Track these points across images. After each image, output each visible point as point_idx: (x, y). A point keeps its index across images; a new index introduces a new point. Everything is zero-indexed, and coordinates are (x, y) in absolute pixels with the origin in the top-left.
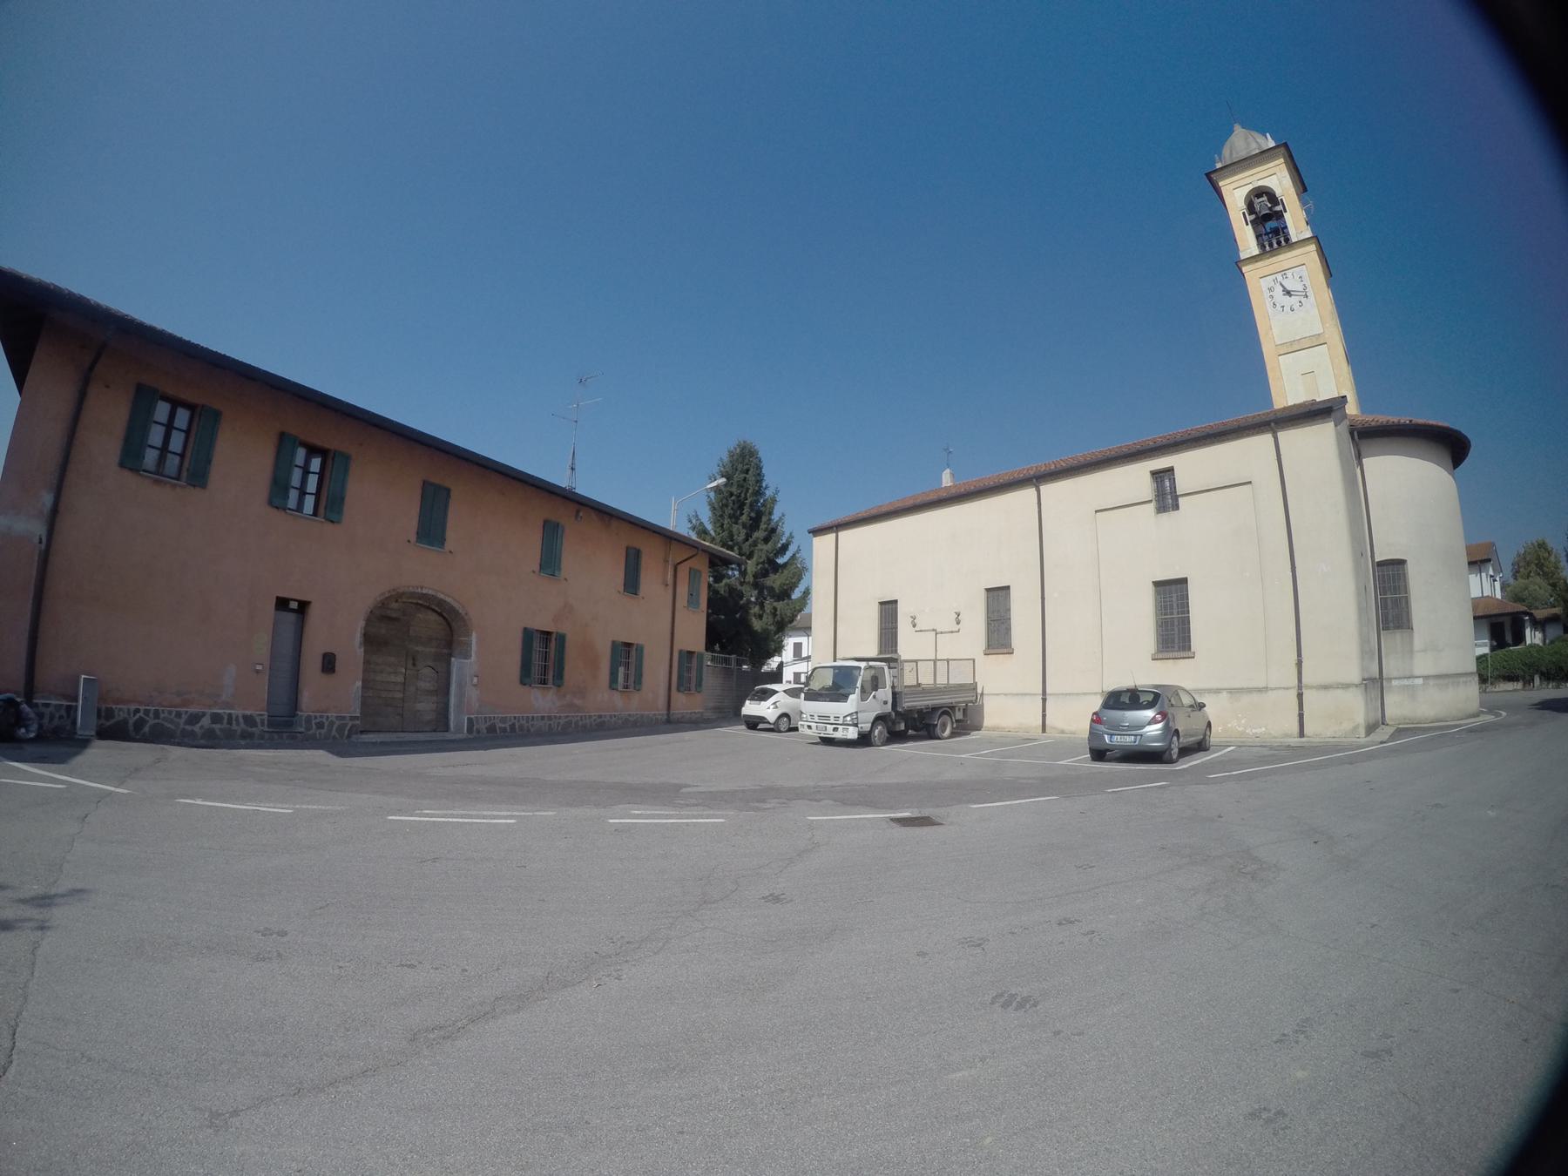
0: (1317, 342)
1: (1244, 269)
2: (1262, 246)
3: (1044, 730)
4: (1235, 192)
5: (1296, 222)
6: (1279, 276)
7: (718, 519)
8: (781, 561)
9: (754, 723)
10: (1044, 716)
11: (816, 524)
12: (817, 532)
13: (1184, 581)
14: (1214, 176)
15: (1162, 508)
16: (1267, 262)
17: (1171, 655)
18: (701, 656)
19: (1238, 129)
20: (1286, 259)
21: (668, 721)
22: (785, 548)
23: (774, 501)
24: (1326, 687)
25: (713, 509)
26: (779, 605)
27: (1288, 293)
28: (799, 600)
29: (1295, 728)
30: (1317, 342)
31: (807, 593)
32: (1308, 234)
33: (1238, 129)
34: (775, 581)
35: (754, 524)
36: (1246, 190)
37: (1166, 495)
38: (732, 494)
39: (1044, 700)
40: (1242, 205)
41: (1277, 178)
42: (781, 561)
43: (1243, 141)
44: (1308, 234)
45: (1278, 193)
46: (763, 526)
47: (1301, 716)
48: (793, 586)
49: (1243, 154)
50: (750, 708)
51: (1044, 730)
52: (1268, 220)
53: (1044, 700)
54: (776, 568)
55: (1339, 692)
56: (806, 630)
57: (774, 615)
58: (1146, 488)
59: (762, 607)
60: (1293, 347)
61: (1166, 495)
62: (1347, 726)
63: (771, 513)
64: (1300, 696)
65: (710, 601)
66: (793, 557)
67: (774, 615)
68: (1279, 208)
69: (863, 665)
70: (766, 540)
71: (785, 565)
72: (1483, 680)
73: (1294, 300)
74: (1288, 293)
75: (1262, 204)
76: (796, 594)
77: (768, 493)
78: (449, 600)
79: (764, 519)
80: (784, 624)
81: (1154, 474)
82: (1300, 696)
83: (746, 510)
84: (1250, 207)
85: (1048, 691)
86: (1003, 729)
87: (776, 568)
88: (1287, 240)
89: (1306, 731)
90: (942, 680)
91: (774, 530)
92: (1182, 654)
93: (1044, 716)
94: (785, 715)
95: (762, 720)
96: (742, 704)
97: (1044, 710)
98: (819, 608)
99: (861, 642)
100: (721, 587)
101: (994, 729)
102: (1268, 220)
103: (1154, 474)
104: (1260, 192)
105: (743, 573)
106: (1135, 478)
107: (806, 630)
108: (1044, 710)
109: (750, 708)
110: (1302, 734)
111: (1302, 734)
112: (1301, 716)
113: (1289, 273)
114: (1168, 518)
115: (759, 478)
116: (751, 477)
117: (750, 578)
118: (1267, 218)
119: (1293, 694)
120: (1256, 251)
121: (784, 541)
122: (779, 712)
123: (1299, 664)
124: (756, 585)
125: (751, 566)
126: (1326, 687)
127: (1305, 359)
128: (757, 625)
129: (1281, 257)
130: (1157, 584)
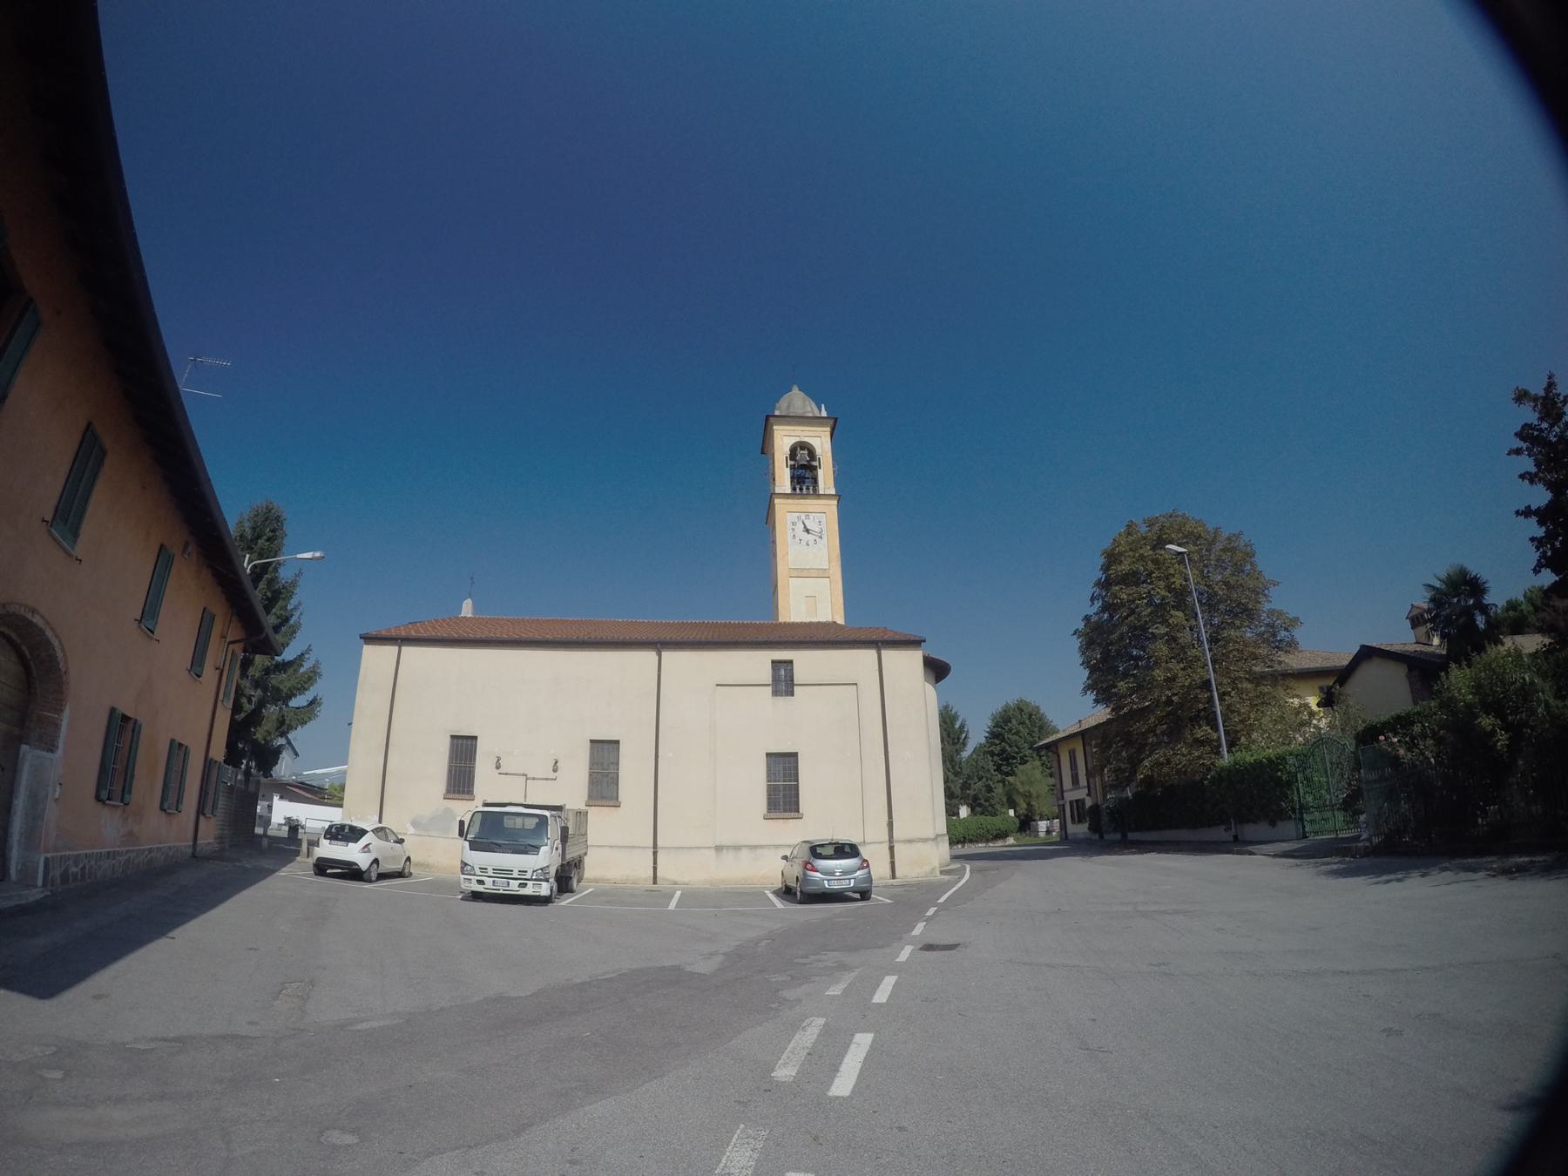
0: (822, 574)
1: (777, 501)
4: (784, 439)
5: (826, 478)
10: (655, 869)
11: (373, 631)
12: (370, 639)
13: (795, 755)
15: (776, 693)
19: (795, 390)
20: (811, 504)
21: (194, 856)
24: (910, 841)
27: (807, 531)
29: (888, 872)
30: (822, 574)
32: (833, 492)
33: (795, 390)
36: (794, 440)
37: (783, 681)
39: (655, 854)
40: (787, 450)
41: (821, 441)
43: (797, 400)
44: (833, 492)
45: (818, 451)
47: (893, 864)
49: (800, 412)
52: (804, 474)
53: (655, 854)
55: (920, 845)
58: (766, 675)
60: (802, 573)
61: (783, 681)
62: (927, 868)
64: (891, 848)
69: (547, 813)
72: (952, 843)
74: (807, 531)
76: (298, 701)
78: (56, 643)
79: (280, 603)
81: (776, 664)
82: (891, 848)
83: (262, 585)
88: (815, 490)
89: (898, 874)
91: (287, 620)
93: (655, 869)
101: (596, 881)
102: (804, 474)
103: (776, 664)
106: (758, 663)
110: (894, 876)
111: (894, 876)
112: (893, 864)
114: (782, 701)
118: (802, 467)
119: (886, 846)
120: (789, 491)
122: (371, 857)
123: (890, 825)
126: (910, 841)
127: (810, 585)
130: (768, 755)
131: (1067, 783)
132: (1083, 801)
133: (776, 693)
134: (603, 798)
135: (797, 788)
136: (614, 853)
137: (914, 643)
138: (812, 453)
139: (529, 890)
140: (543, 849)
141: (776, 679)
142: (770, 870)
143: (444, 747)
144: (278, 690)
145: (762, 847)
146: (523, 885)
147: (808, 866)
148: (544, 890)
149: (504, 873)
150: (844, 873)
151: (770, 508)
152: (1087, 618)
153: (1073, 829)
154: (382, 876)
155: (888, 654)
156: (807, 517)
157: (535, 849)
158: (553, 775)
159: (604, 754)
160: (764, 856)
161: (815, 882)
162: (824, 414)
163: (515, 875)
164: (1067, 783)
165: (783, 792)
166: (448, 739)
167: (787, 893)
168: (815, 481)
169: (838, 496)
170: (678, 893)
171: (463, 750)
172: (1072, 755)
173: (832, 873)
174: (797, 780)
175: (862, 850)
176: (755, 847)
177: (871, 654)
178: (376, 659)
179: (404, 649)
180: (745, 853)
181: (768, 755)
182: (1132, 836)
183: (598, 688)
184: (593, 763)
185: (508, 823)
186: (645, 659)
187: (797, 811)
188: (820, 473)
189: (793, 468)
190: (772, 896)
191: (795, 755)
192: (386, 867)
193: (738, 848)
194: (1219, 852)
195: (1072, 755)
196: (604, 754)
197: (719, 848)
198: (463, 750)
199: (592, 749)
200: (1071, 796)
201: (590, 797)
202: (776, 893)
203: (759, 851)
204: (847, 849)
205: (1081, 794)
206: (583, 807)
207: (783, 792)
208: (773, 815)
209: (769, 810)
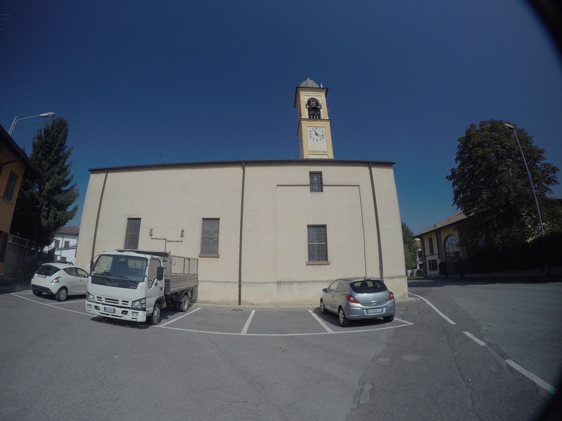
2: (310, 117)
3: (240, 304)
4: (304, 97)
5: (324, 113)
6: (314, 128)
7: (36, 153)
8: (63, 189)
9: (41, 292)
10: (240, 295)
12: (94, 171)
13: (324, 226)
14: (299, 89)
16: (308, 122)
17: (320, 262)
18: (6, 236)
19: (308, 79)
20: (318, 123)
22: (67, 182)
23: (69, 153)
24: (392, 278)
25: (35, 146)
26: (59, 213)
27: (317, 135)
28: (71, 212)
31: (76, 209)
34: (59, 198)
35: (54, 163)
38: (47, 142)
39: (240, 286)
40: (306, 101)
41: (321, 98)
42: (63, 189)
43: (310, 83)
45: (320, 102)
46: (60, 165)
48: (69, 204)
50: (38, 280)
51: (240, 304)
52: (314, 110)
53: (240, 286)
54: (61, 192)
56: (75, 234)
57: (55, 218)
58: (307, 181)
59: (48, 212)
63: (66, 159)
65: (18, 201)
66: (72, 188)
67: (55, 218)
68: (319, 107)
69: (148, 257)
70: (59, 174)
71: (66, 191)
73: (318, 138)
74: (317, 135)
75: (313, 104)
76: (70, 209)
77: (66, 150)
79: (61, 161)
80: (57, 226)
81: (312, 174)
83: (53, 153)
84: (309, 102)
85: (242, 280)
86: (211, 302)
87: (61, 192)
88: (319, 118)
90: (186, 272)
91: (65, 169)
92: (324, 262)
93: (240, 295)
94: (64, 288)
95: (47, 290)
96: (32, 277)
97: (240, 291)
98: (86, 220)
99: (113, 243)
100: (27, 193)
101: (205, 302)
102: (314, 110)
103: (312, 174)
104: (313, 100)
105: (41, 191)
106: (301, 173)
107: (75, 234)
108: (240, 291)
109: (38, 280)
113: (318, 128)
114: (316, 195)
115: (65, 138)
116: (61, 136)
117: (44, 193)
120: (308, 117)
121: (67, 178)
122: (59, 286)
124: (47, 198)
125: (48, 186)
126: (392, 278)
128: (44, 223)
129: (317, 122)
130: (309, 226)
131: (428, 252)
132: (435, 261)
133: (312, 190)
134: (210, 252)
135: (326, 246)
136: (214, 286)
137: (388, 164)
138: (317, 103)
139: (128, 317)
140: (141, 285)
141: (312, 183)
142: (312, 297)
143: (124, 224)
144: (57, 202)
145: (305, 282)
146: (125, 313)
147: (349, 298)
148: (141, 317)
149: (112, 301)
150: (378, 303)
151: (299, 126)
152: (453, 170)
153: (429, 273)
154: (69, 298)
155: (375, 170)
156: (316, 129)
157: (133, 285)
158: (181, 239)
159: (211, 225)
160: (310, 288)
161: (356, 312)
162: (322, 87)
163: (120, 304)
164: (428, 252)
165: (318, 251)
166: (126, 221)
167: (327, 314)
168: (319, 115)
169: (330, 120)
170: (253, 312)
171: (134, 224)
172: (430, 240)
173: (370, 304)
174: (326, 241)
175: (386, 282)
176: (300, 282)
177: (364, 170)
178: (96, 180)
179: (109, 174)
180: (295, 286)
181: (309, 226)
182: (466, 276)
183: (207, 189)
184: (204, 232)
185: (131, 263)
186: (237, 171)
187: (327, 260)
188: (321, 110)
189: (309, 109)
190: (314, 315)
191: (324, 226)
192: (72, 292)
193: (290, 283)
194: (505, 282)
195: (430, 240)
196: (211, 225)
197: (279, 283)
198: (134, 224)
199: (203, 224)
200: (429, 259)
201: (202, 252)
202: (317, 311)
203: (304, 285)
204: (370, 284)
205: (435, 257)
206: (197, 257)
207: (318, 251)
208: (311, 263)
209: (309, 259)
